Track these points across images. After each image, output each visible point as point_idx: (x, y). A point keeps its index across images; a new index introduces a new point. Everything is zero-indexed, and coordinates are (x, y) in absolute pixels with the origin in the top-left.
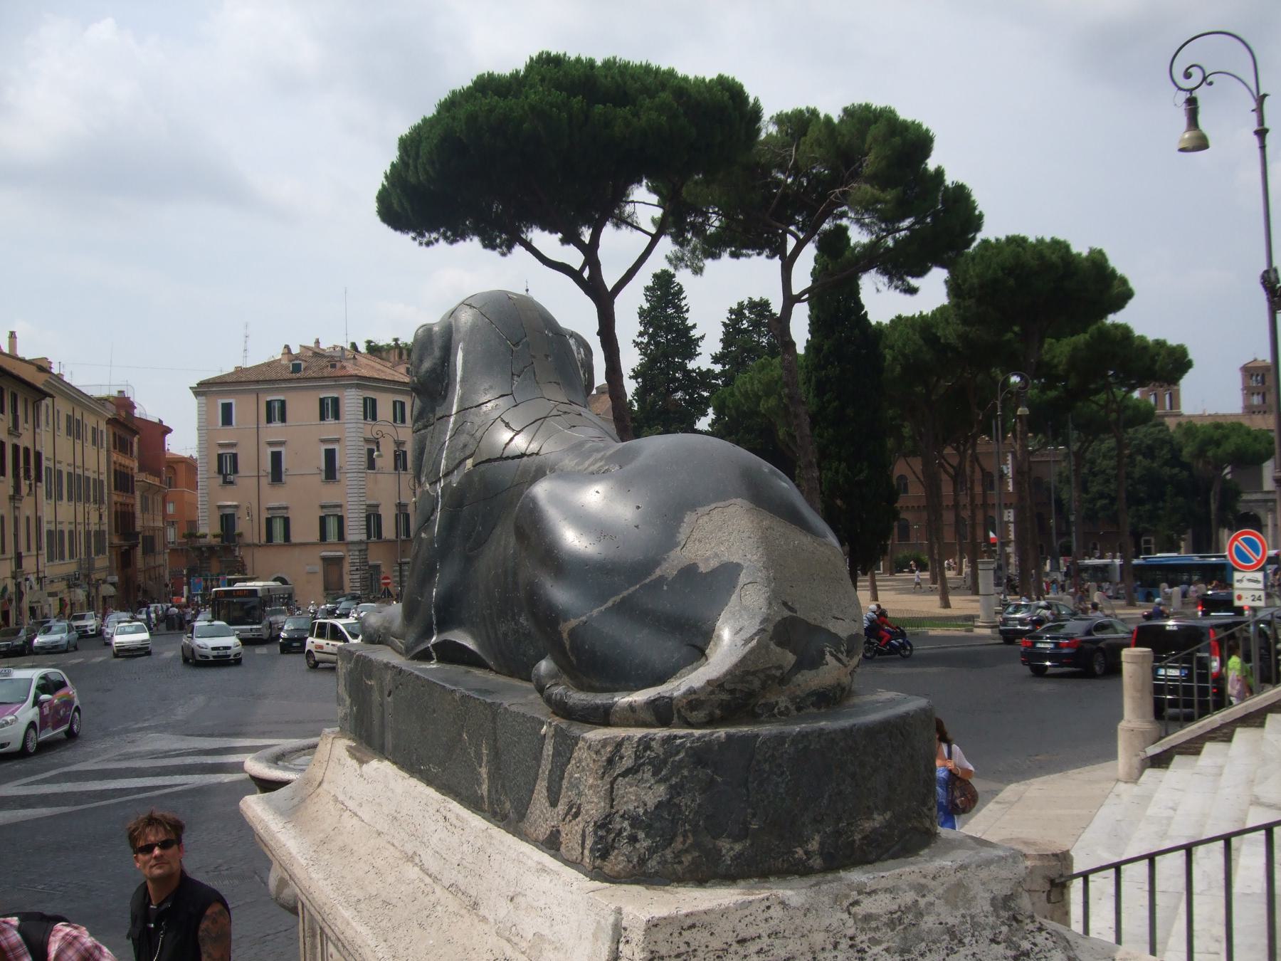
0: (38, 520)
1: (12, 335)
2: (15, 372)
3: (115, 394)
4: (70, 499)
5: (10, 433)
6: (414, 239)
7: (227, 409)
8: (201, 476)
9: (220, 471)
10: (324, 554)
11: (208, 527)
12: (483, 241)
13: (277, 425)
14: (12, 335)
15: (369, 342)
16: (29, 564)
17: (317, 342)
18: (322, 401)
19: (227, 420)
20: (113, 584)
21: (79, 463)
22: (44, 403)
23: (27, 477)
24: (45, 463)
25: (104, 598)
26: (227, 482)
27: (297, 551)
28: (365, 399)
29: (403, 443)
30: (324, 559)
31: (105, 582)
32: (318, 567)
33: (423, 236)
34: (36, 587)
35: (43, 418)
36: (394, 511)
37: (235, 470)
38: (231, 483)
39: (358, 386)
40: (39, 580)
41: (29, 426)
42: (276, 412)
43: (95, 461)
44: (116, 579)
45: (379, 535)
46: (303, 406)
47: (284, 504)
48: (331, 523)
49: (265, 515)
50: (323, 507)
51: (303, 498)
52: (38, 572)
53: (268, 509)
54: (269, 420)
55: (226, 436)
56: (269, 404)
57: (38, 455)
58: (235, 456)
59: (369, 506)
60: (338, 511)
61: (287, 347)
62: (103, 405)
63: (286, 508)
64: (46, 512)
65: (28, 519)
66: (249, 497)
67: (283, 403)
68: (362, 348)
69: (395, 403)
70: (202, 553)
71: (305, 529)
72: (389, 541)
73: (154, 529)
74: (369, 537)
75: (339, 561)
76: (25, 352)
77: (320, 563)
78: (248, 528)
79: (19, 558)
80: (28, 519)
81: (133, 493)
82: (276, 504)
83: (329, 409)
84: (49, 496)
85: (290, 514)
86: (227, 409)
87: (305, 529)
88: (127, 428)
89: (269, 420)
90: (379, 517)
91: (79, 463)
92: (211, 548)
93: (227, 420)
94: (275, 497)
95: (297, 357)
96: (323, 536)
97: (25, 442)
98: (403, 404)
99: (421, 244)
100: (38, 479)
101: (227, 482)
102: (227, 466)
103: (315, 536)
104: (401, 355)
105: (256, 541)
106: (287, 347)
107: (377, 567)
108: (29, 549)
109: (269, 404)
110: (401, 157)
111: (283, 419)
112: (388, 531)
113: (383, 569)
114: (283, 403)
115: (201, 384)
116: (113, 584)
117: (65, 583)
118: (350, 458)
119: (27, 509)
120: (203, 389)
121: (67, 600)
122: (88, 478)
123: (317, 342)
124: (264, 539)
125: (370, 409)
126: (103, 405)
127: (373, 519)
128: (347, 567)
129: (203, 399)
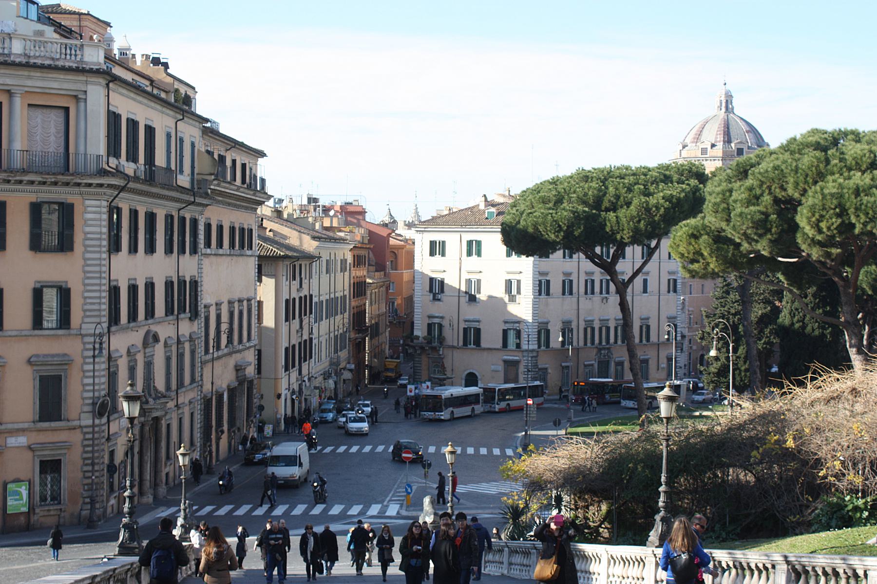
9: (431, 290)
10: (506, 357)
20: (351, 370)
26: (435, 299)
27: (485, 353)
29: (570, 274)
30: (505, 361)
32: (501, 367)
38: (439, 300)
49: (463, 325)
53: (466, 321)
60: (475, 325)
63: (478, 321)
74: (539, 347)
75: (516, 363)
77: (502, 363)
78: (453, 336)
82: (471, 318)
101: (435, 299)
103: (499, 345)
105: (455, 344)
111: (479, 254)
113: (549, 371)
116: (351, 370)
124: (461, 343)
128: (522, 369)
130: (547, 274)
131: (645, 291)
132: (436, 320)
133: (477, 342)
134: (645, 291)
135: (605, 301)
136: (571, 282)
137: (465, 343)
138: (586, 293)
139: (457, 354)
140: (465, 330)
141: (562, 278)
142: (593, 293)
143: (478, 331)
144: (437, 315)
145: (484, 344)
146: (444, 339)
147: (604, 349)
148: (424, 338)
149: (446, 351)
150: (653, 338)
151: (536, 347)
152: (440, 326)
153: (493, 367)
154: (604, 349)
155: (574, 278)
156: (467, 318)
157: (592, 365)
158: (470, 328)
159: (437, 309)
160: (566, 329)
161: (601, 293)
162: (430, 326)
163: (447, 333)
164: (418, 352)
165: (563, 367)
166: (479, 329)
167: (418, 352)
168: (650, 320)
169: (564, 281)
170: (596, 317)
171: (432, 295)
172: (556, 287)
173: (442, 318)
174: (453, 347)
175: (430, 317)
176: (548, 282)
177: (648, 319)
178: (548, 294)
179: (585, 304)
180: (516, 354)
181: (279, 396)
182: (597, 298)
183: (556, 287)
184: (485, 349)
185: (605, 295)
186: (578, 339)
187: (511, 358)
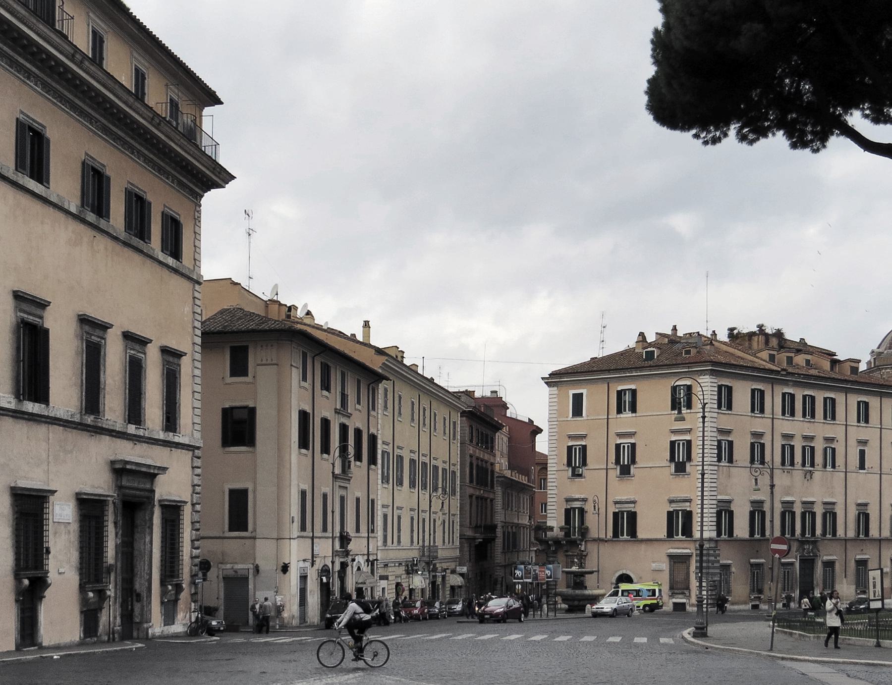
0: (372, 504)
1: (367, 324)
2: (356, 357)
3: (489, 394)
4: (412, 484)
5: (337, 412)
6: (696, 136)
7: (578, 399)
8: (552, 467)
9: (569, 464)
10: (672, 551)
11: (555, 520)
12: (789, 135)
13: (627, 415)
14: (367, 324)
15: (731, 330)
16: (356, 546)
17: (675, 329)
18: (674, 389)
19: (577, 410)
20: (462, 575)
21: (424, 450)
22: (381, 386)
23: (358, 457)
24: (380, 447)
25: (452, 588)
26: (576, 475)
27: (643, 546)
28: (720, 387)
29: (760, 435)
30: (671, 557)
31: (453, 572)
32: (665, 566)
33: (709, 132)
34: (365, 568)
35: (380, 401)
36: (748, 508)
37: (584, 463)
38: (580, 476)
39: (713, 373)
40: (371, 563)
41: (363, 407)
42: (627, 403)
43: (445, 449)
44: (464, 570)
45: (731, 532)
46: (654, 394)
47: (632, 497)
48: (679, 522)
49: (612, 509)
50: (671, 501)
51: (652, 493)
52: (368, 555)
53: (616, 503)
54: (619, 411)
55: (578, 426)
56: (620, 394)
57: (373, 439)
58: (584, 448)
59: (719, 501)
60: (630, 507)
61: (642, 334)
62: (459, 398)
63: (634, 502)
64: (382, 494)
65: (358, 500)
66: (600, 491)
67: (634, 392)
68: (723, 336)
69: (753, 391)
70: (549, 546)
71: (653, 524)
72: (742, 541)
73: (518, 526)
74: (719, 534)
75: (685, 558)
76: (378, 341)
77: (667, 560)
78: (598, 524)
79: (345, 539)
80: (358, 500)
81: (492, 487)
82: (624, 498)
83: (681, 401)
84: (385, 479)
85: (638, 509)
86: (578, 399)
87: (653, 524)
88: (483, 417)
89: (619, 411)
90: (731, 514)
91: (424, 450)
92: (557, 542)
93: (577, 410)
94: (623, 491)
95: (650, 345)
96: (670, 533)
97: (356, 422)
98: (762, 393)
99: (706, 143)
100: (373, 460)
101: (576, 475)
102: (577, 459)
103: (662, 533)
104: (767, 342)
105: (603, 536)
106: (642, 334)
107: (726, 567)
108: (358, 530)
109: (620, 394)
110: (666, 25)
111: (633, 409)
112: (741, 529)
113: (733, 569)
114: (634, 392)
115: (553, 375)
116: (462, 575)
117: (403, 568)
118: (704, 451)
119: (356, 490)
120: (556, 379)
121: (405, 585)
122: (436, 468)
123: (675, 329)
124: (610, 534)
125: (725, 399)
126: (459, 398)
127: (725, 513)
129: (555, 390)
130: (729, 432)
131: (862, 466)
132: (577, 504)
133: (633, 532)
134: (862, 466)
135: (808, 476)
136: (763, 446)
137: (616, 534)
138: (783, 464)
139: (605, 549)
140: (615, 515)
141: (749, 440)
142: (792, 464)
143: (633, 516)
144: (577, 496)
145: (641, 535)
146: (587, 529)
147: (808, 542)
148: (561, 529)
149: (589, 545)
150: (874, 532)
151: (714, 534)
152: (582, 511)
153: (654, 566)
154: (808, 542)
155: (766, 440)
156: (618, 498)
157: (792, 564)
158: (622, 512)
159: (577, 490)
160: (757, 512)
161: (804, 465)
162: (568, 512)
163: (591, 520)
164: (553, 548)
165: (752, 565)
166: (635, 513)
167: (553, 548)
168: (869, 507)
169: (752, 445)
170: (797, 498)
171: (570, 469)
172: (742, 453)
173: (585, 500)
174: (599, 540)
175: (568, 500)
176: (731, 443)
177: (866, 505)
178: (731, 460)
179: (781, 479)
180: (685, 545)
181: (285, 569)
182: (798, 475)
183: (742, 453)
184: (642, 541)
185: (808, 468)
186: (774, 528)
187: (679, 551)
